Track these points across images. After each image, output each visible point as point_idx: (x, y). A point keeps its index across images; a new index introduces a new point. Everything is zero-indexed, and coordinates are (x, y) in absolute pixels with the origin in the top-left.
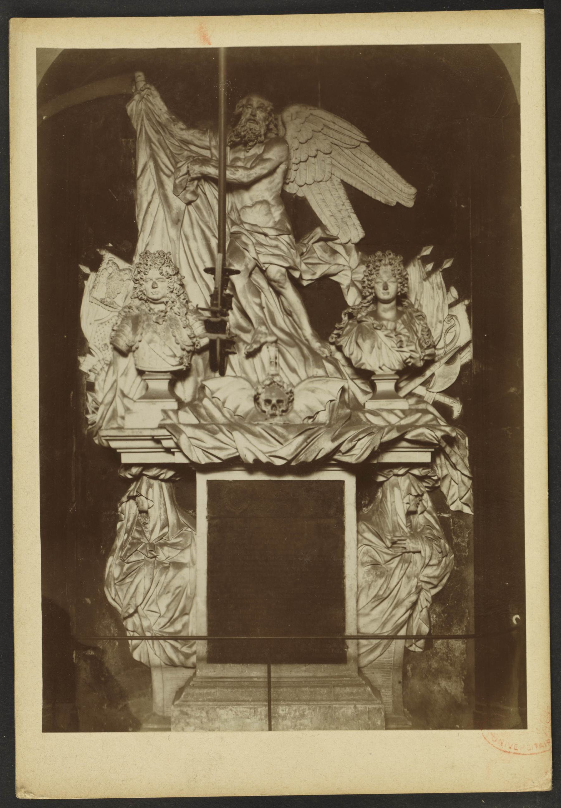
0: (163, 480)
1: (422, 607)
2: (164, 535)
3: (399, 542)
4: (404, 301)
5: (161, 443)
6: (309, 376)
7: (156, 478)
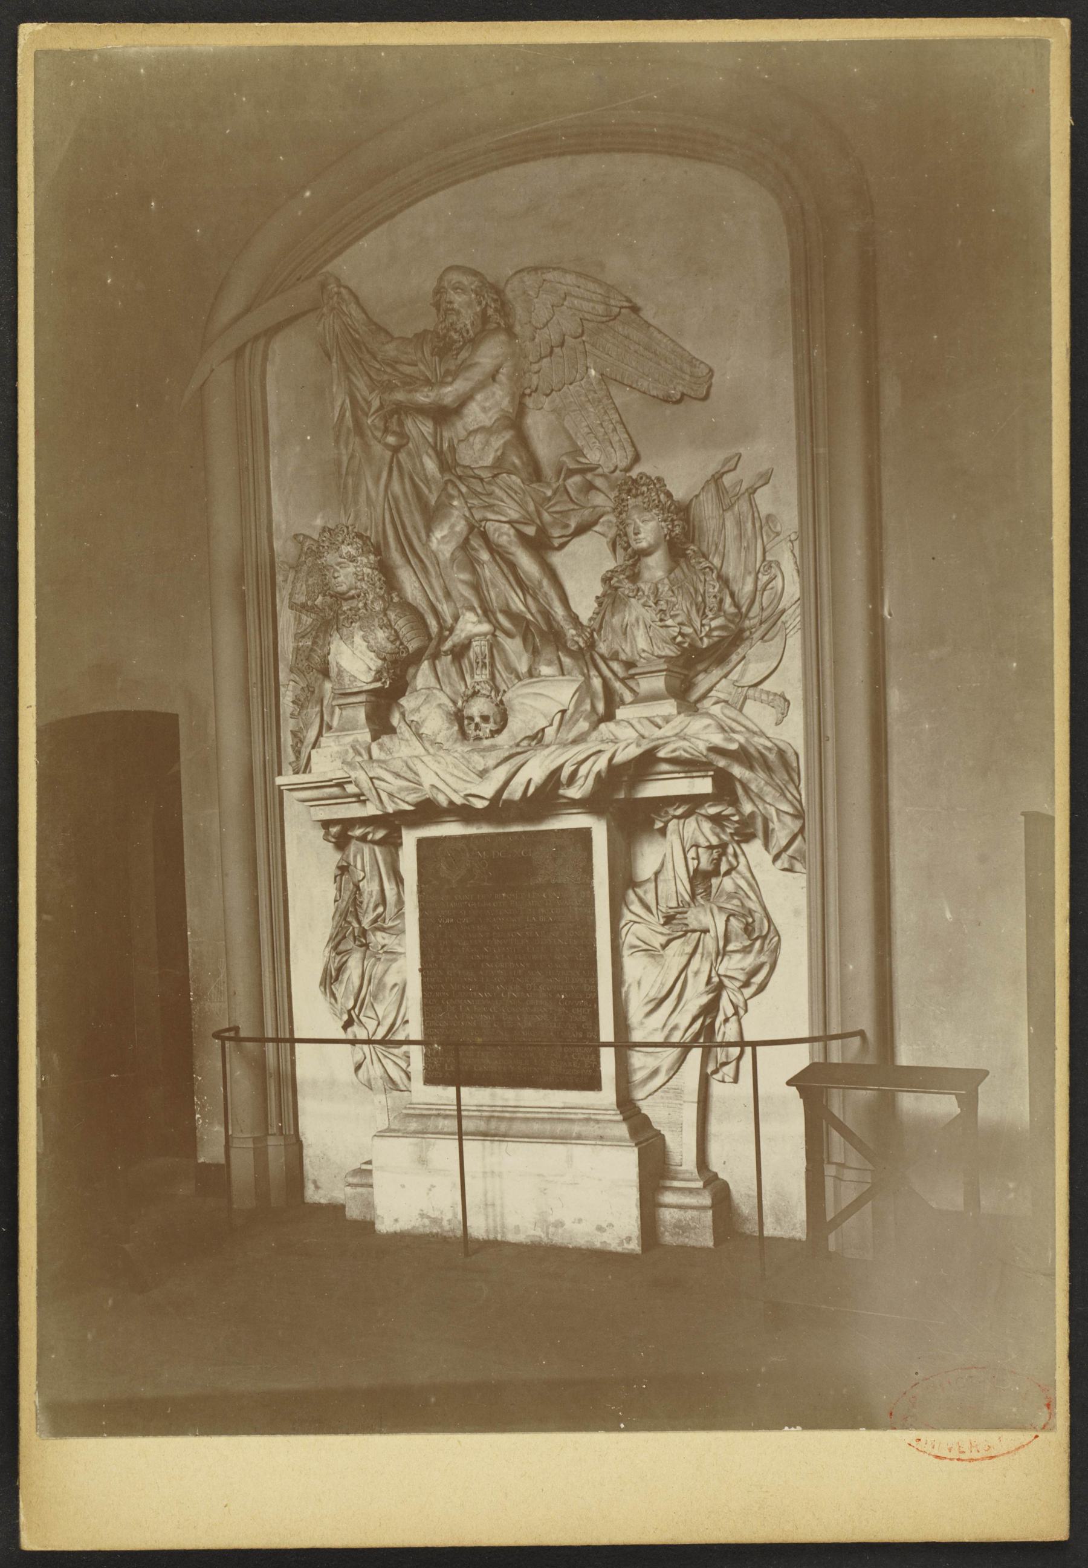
0: (374, 842)
1: (725, 1014)
2: (379, 916)
3: (678, 916)
4: (687, 549)
5: (344, 789)
6: (748, 701)
7: (363, 839)
